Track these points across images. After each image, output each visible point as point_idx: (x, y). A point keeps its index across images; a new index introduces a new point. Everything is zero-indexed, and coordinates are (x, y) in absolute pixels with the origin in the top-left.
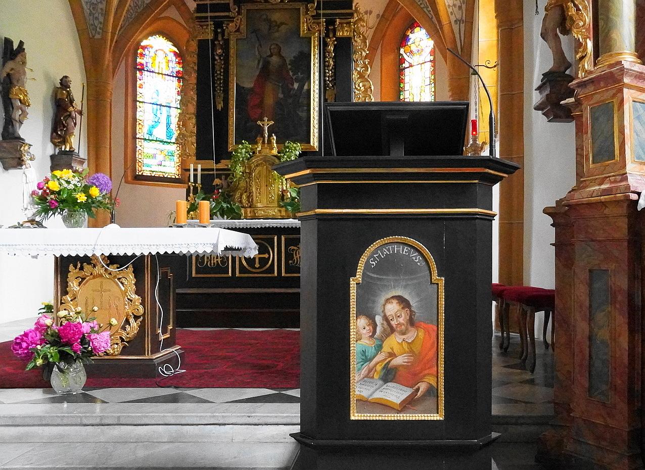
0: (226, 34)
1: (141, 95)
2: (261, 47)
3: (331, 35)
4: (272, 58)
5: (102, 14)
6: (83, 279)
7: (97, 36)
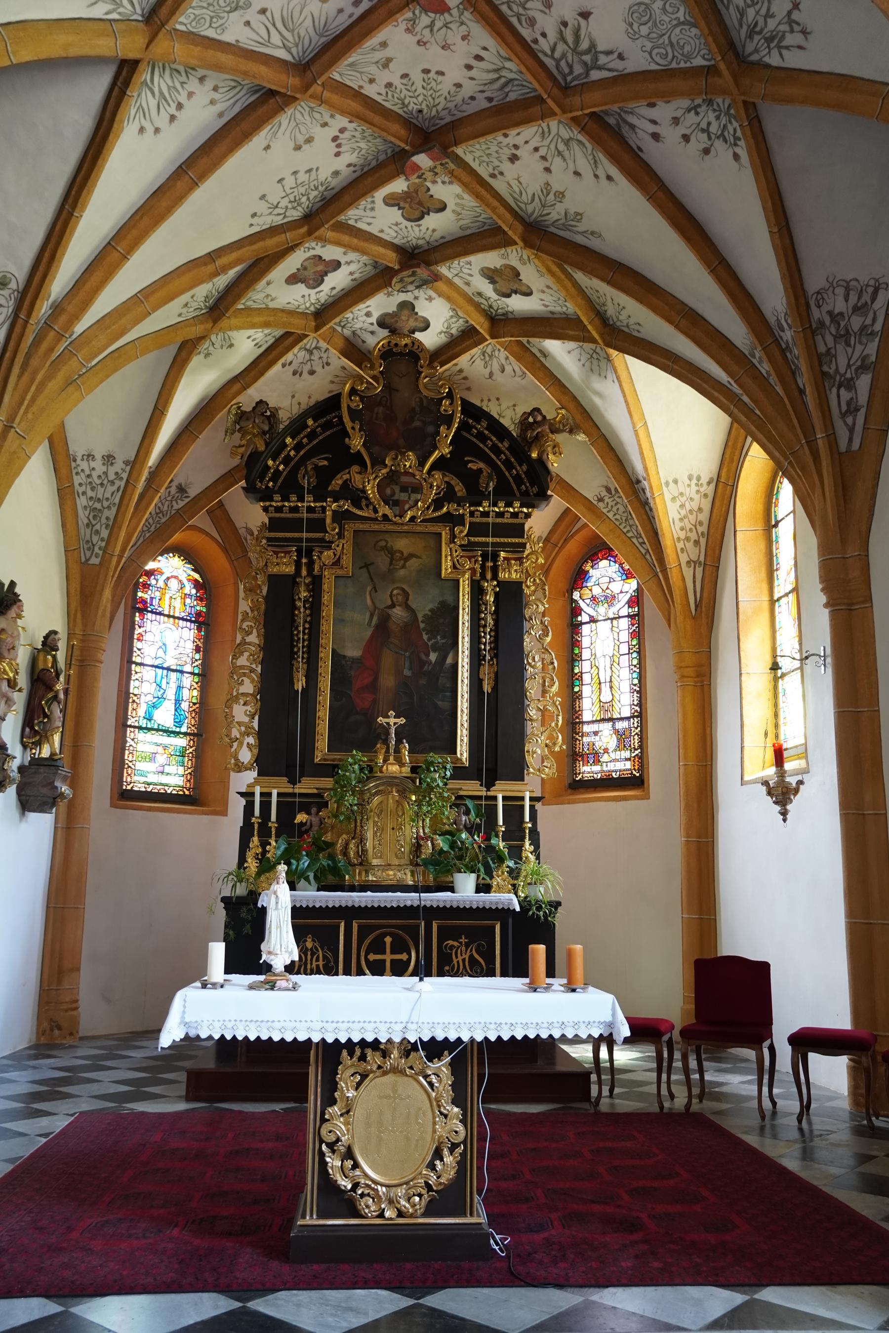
0: (317, 567)
1: (139, 652)
2: (376, 591)
3: (489, 576)
4: (394, 610)
5: (107, 526)
6: (364, 1077)
7: (95, 561)
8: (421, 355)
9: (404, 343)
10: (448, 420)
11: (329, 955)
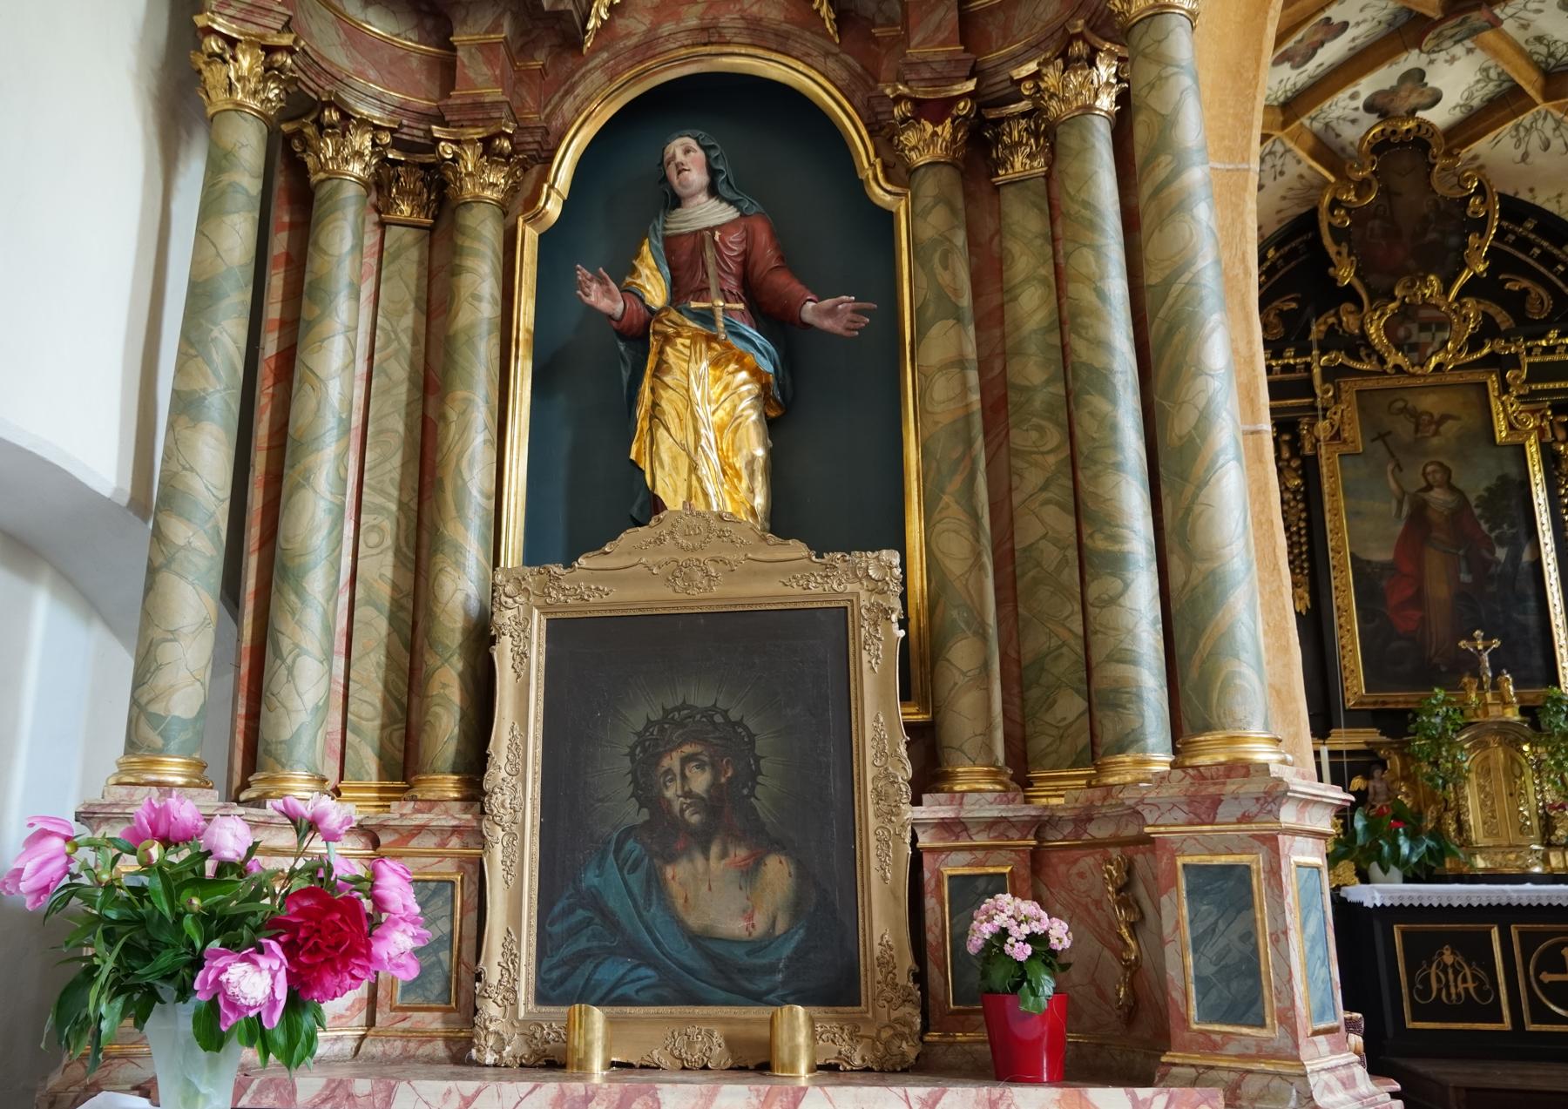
8: (1431, 141)
9: (1405, 128)
10: (1481, 226)
11: (1482, 974)
